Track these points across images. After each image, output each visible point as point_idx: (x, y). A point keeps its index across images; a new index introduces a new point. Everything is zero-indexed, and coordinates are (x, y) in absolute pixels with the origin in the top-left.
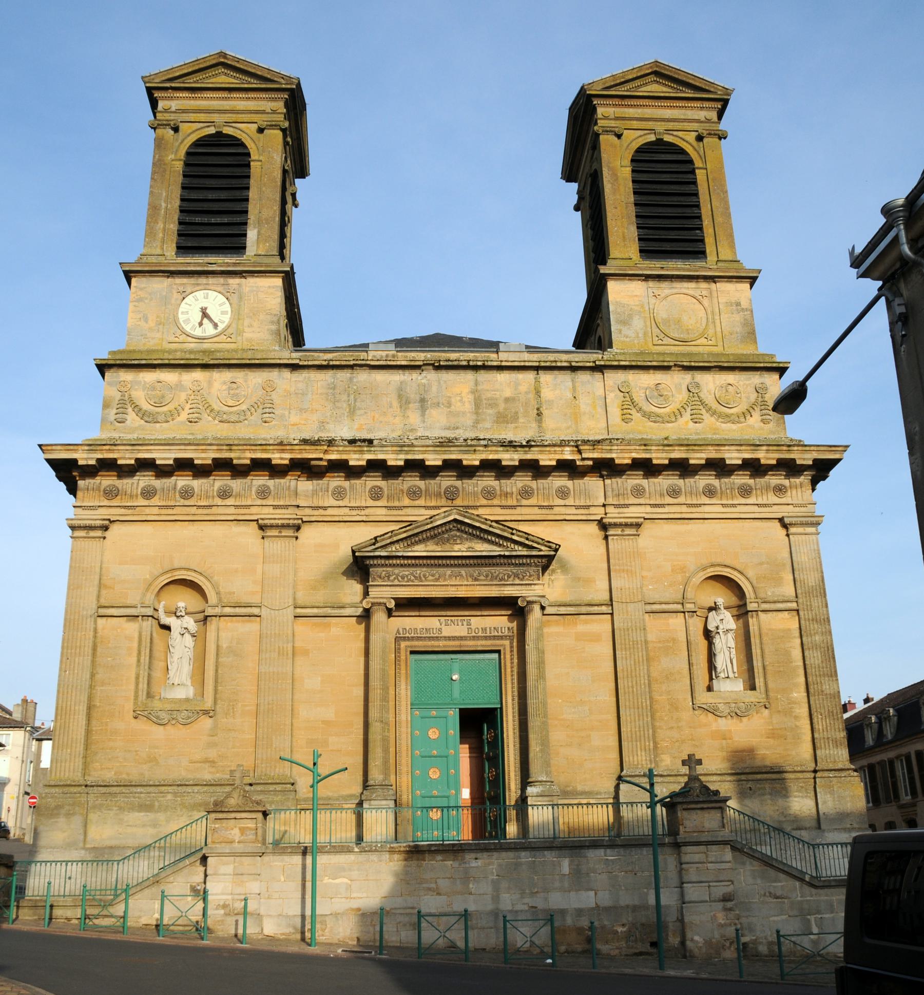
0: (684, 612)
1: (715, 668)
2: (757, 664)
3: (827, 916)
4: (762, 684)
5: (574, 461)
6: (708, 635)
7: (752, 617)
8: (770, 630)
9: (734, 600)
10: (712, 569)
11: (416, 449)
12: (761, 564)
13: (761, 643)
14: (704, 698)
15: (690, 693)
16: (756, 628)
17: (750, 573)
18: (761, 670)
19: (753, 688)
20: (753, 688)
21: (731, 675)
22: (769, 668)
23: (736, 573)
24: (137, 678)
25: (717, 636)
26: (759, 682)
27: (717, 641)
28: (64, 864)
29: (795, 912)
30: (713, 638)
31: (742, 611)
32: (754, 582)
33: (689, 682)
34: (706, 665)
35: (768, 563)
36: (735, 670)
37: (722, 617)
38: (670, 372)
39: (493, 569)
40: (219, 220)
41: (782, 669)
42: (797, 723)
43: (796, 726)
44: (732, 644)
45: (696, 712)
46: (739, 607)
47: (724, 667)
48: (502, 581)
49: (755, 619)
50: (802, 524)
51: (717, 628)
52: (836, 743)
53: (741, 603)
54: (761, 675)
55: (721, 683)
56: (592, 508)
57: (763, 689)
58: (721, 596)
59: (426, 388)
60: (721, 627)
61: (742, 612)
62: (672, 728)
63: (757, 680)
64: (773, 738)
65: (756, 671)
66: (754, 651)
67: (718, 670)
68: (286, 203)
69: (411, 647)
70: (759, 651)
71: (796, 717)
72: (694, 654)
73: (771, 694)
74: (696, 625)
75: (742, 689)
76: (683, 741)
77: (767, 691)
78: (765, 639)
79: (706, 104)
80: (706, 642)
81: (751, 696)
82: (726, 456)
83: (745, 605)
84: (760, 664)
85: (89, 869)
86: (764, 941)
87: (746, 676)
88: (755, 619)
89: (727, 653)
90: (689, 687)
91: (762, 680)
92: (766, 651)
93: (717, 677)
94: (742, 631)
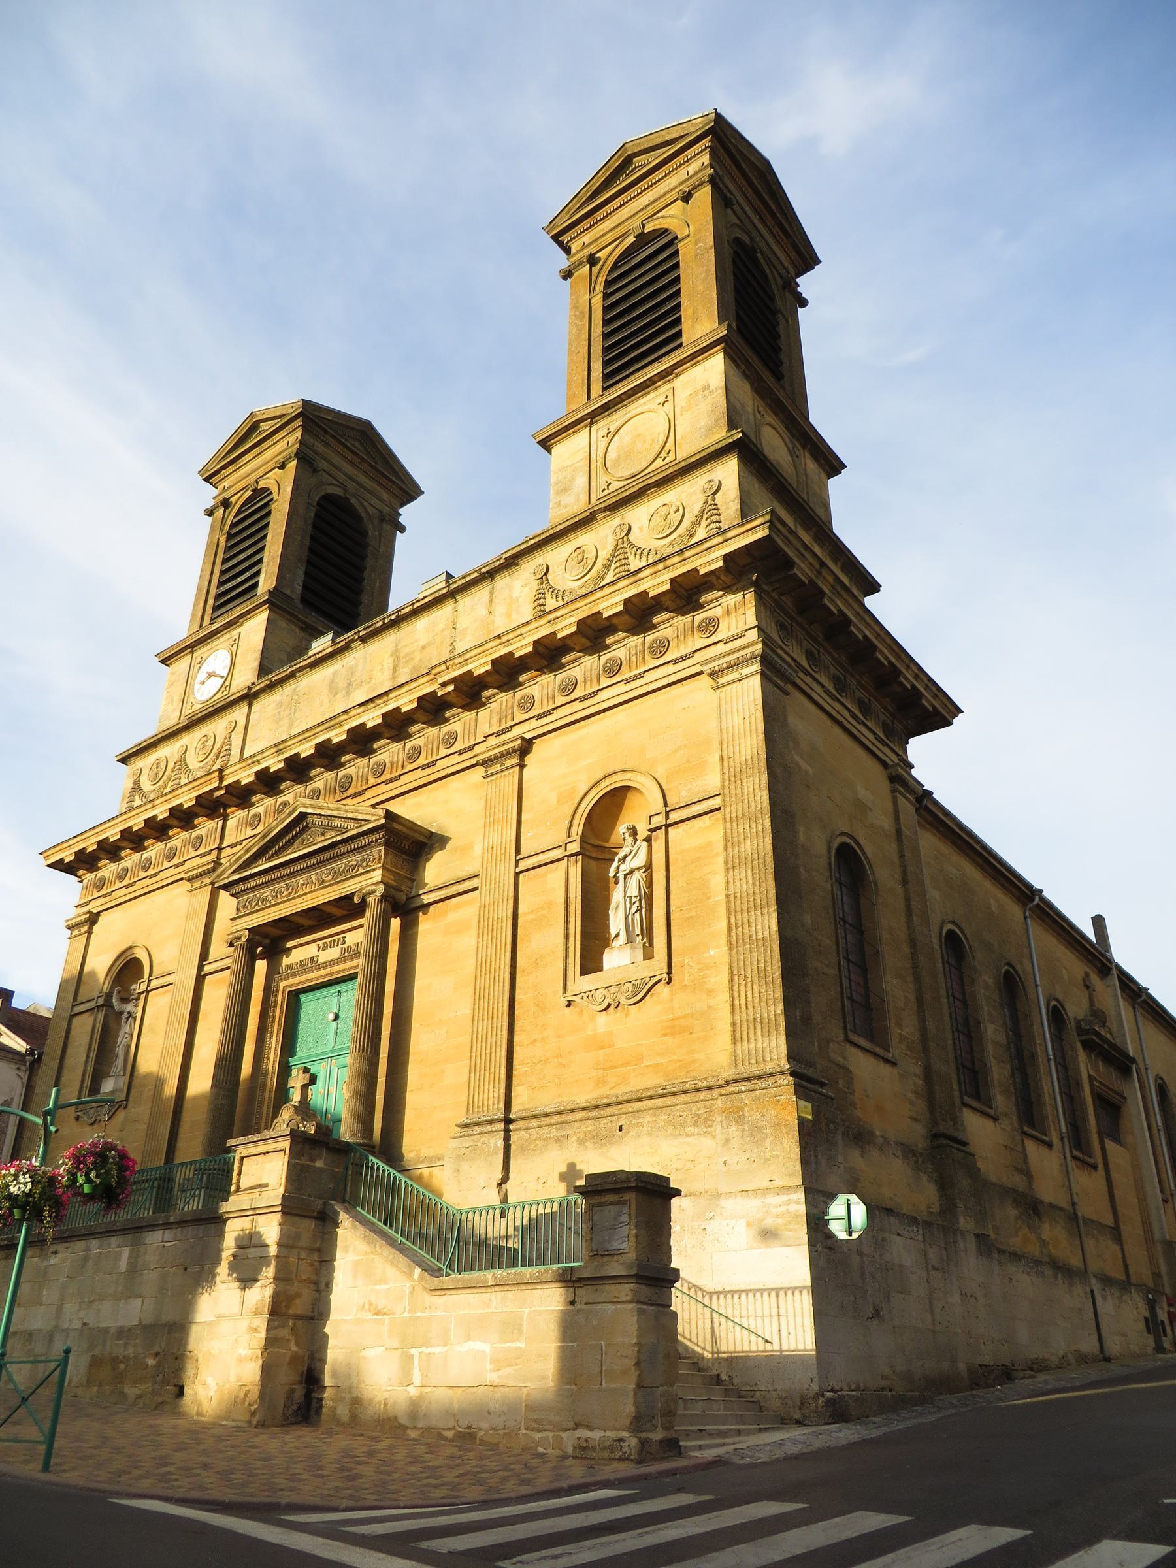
3: (437, 1350)
5: (434, 692)
11: (290, 743)
24: (84, 1075)
28: (773, 1294)
29: (396, 1344)
38: (594, 525)
39: (336, 865)
40: (243, 577)
41: (693, 913)
42: (712, 1002)
43: (709, 1007)
48: (339, 877)
50: (730, 667)
52: (767, 1027)
56: (476, 748)
59: (352, 670)
62: (535, 1041)
64: (673, 1034)
69: (289, 986)
71: (710, 992)
76: (547, 1061)
79: (690, 152)
82: (600, 607)
85: (759, 1303)
86: (348, 1396)
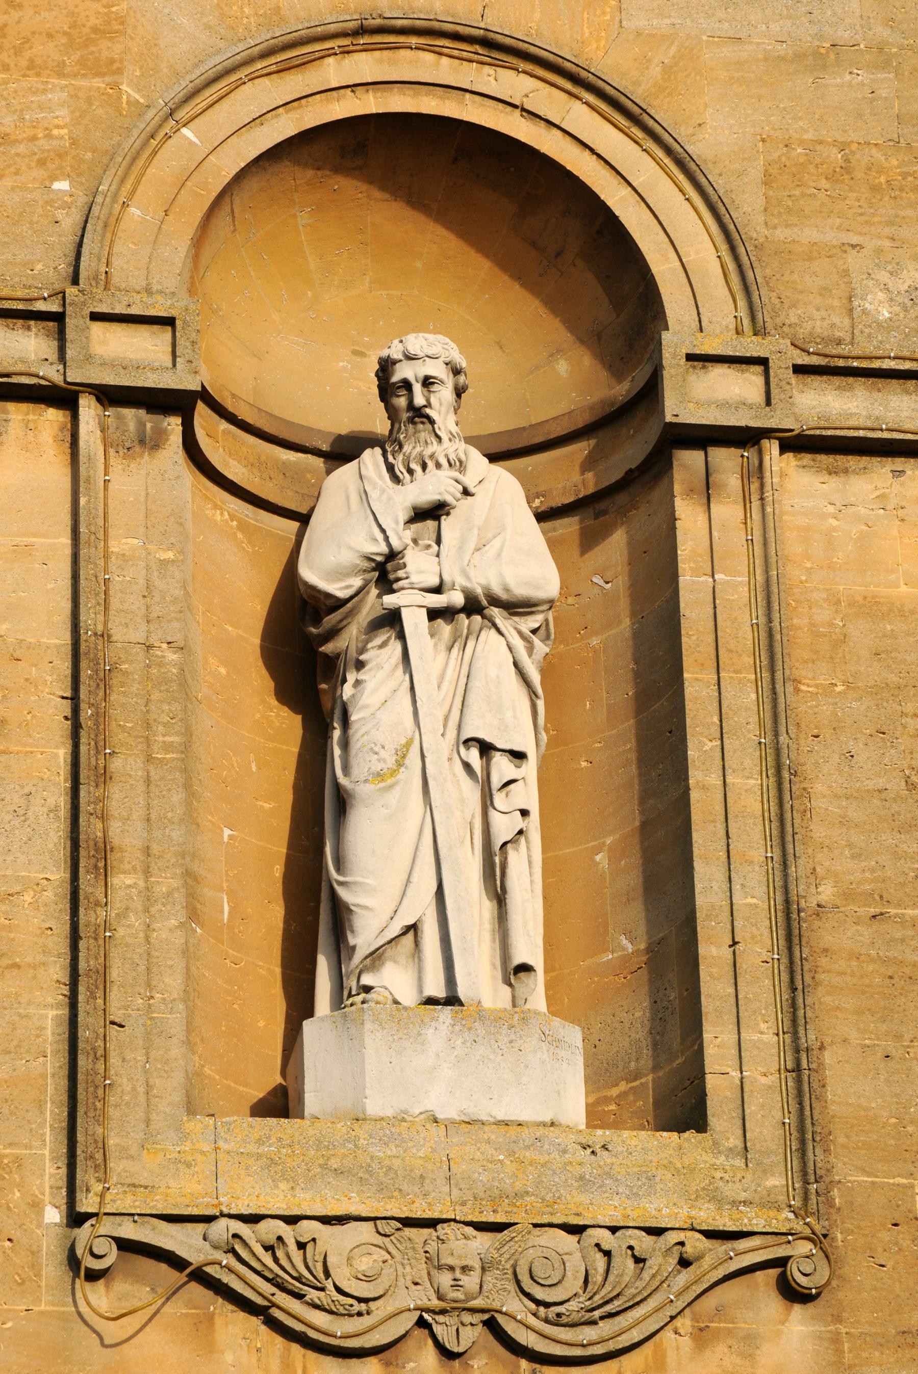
0: (64, 398)
1: (341, 917)
2: (730, 889)
4: (765, 1073)
6: (306, 649)
7: (707, 489)
8: (872, 608)
9: (565, 380)
10: (365, 65)
12: (822, 58)
13: (775, 715)
14: (184, 1160)
15: (52, 1114)
16: (736, 584)
17: (716, 132)
18: (760, 946)
19: (684, 1108)
20: (684, 1108)
21: (479, 979)
22: (838, 940)
23: (580, 116)
25: (383, 656)
26: (740, 1051)
27: (375, 695)
30: (332, 669)
31: (631, 451)
32: (748, 207)
33: (50, 1016)
34: (274, 915)
35: (881, 57)
36: (528, 947)
37: (430, 487)
44: (511, 719)
45: (98, 1297)
46: (604, 424)
47: (420, 906)
49: (727, 511)
51: (385, 571)
53: (622, 390)
54: (762, 991)
55: (375, 1041)
57: (768, 1119)
58: (468, 337)
60: (419, 567)
61: (623, 464)
63: (717, 1040)
65: (712, 951)
66: (702, 777)
67: (365, 935)
68: (308, 1011)
70: (749, 785)
72: (126, 764)
73: (848, 1171)
74: (189, 564)
75: (573, 1104)
77: (805, 1133)
78: (815, 687)
80: (289, 725)
81: (660, 1181)
83: (651, 392)
84: (754, 896)
87: (633, 1013)
88: (727, 511)
89: (458, 795)
90: (52, 1065)
91: (764, 1034)
92: (824, 782)
93: (339, 998)
94: (612, 637)
